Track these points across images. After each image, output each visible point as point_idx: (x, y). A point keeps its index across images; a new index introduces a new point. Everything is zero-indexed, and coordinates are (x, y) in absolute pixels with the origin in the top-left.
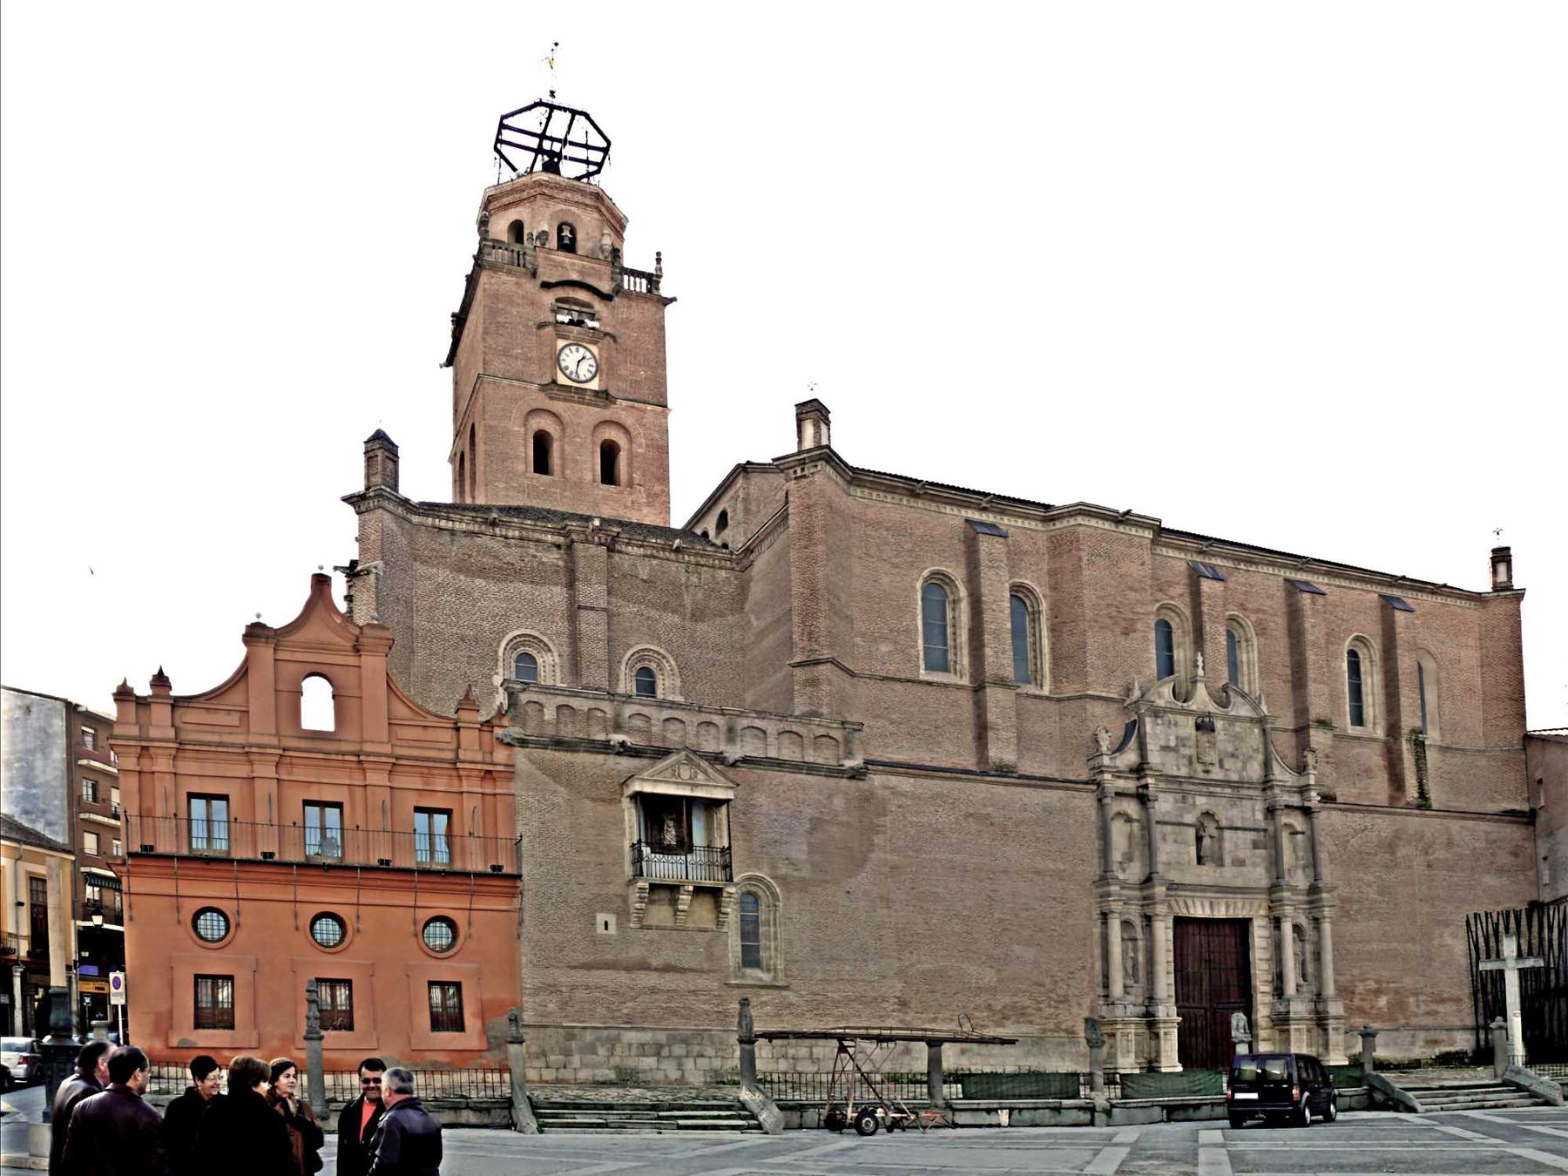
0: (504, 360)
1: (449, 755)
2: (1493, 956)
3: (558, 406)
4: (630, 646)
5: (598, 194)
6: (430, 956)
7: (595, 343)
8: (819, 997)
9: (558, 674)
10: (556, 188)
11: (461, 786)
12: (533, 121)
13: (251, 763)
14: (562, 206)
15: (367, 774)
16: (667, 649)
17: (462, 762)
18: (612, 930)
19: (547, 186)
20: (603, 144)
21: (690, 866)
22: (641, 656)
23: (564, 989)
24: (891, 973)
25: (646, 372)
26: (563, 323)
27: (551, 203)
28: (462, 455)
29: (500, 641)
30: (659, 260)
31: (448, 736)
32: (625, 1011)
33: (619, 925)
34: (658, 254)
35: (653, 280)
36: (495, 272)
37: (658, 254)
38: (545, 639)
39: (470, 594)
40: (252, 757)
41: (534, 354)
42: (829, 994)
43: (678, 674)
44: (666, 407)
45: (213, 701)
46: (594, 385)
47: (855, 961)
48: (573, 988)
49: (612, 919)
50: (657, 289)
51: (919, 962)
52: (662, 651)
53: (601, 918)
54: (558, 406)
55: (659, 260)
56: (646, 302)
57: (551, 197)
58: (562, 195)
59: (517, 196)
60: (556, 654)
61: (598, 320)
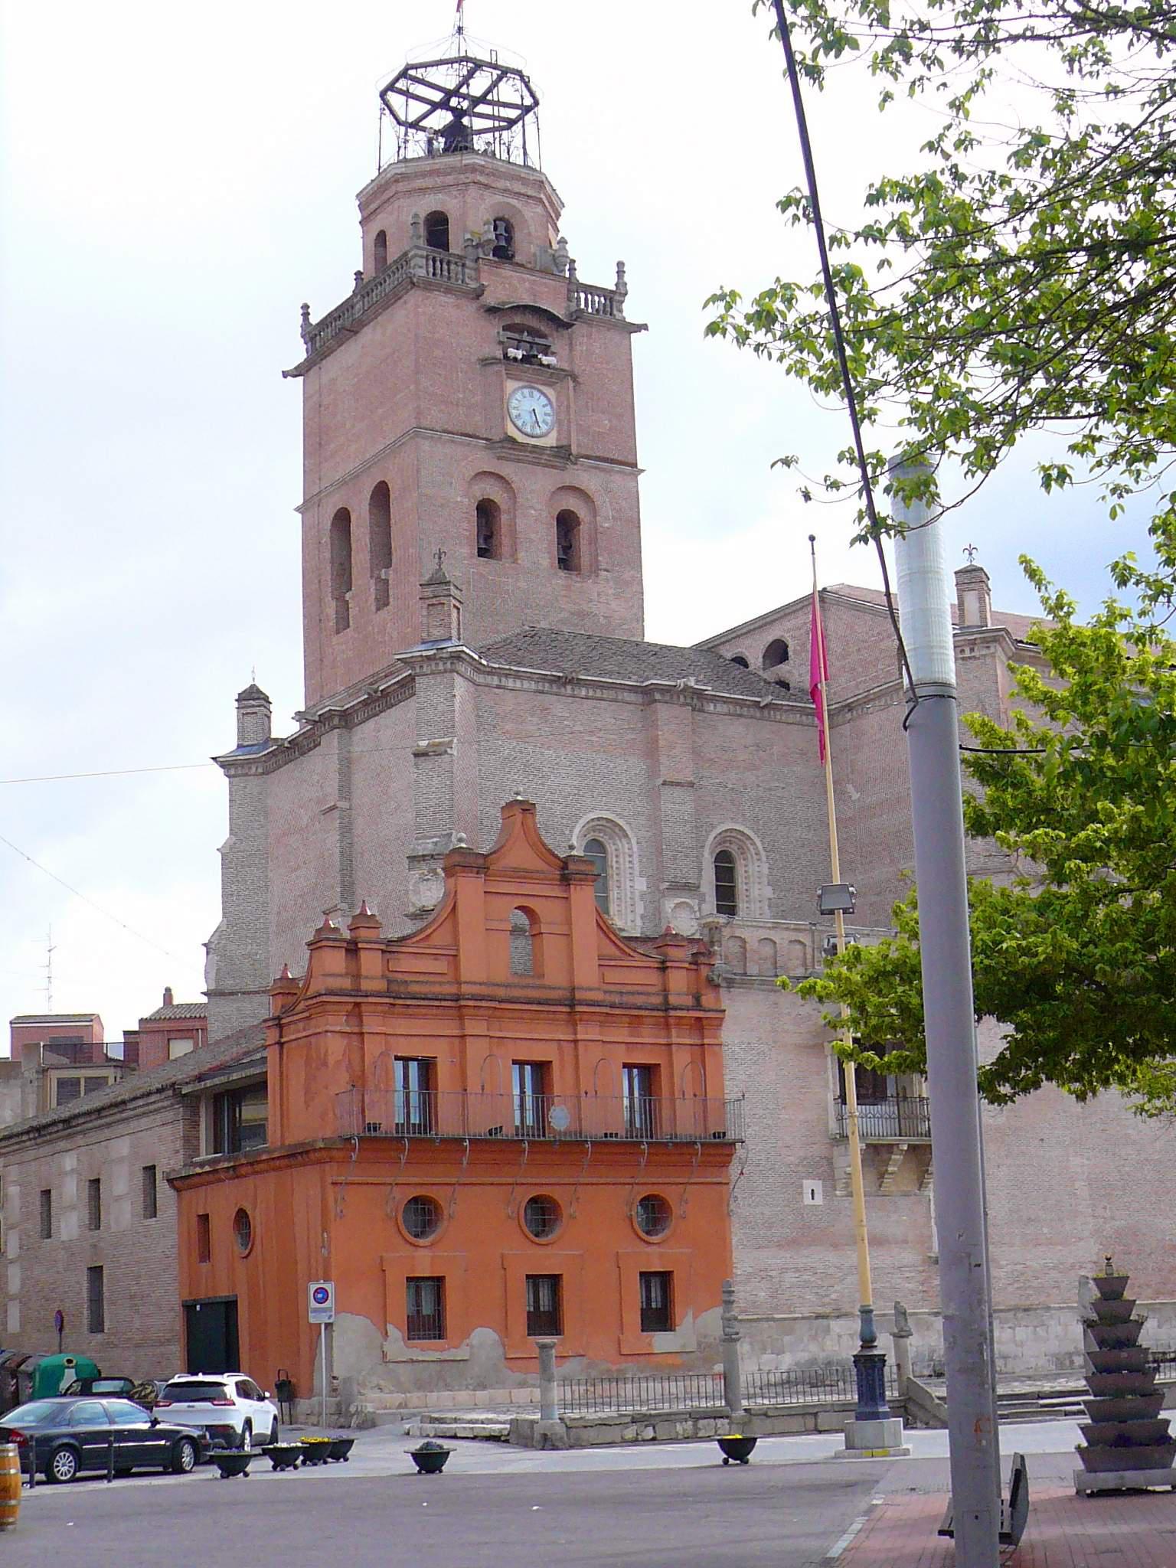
0: (443, 407)
1: (657, 1000)
2: (312, 947)
3: (507, 469)
4: (713, 827)
5: (542, 182)
6: (640, 1238)
7: (550, 385)
8: (1019, 1267)
9: (637, 866)
10: (494, 175)
11: (669, 1036)
12: (447, 78)
13: (461, 1018)
14: (499, 198)
15: (579, 1028)
16: (752, 829)
17: (675, 1009)
18: (819, 1200)
19: (482, 173)
20: (528, 101)
21: (902, 1121)
22: (726, 837)
23: (773, 1273)
24: (1086, 1233)
25: (610, 421)
26: (515, 359)
27: (487, 193)
28: (343, 518)
29: (574, 827)
30: (620, 273)
31: (653, 978)
32: (833, 1296)
33: (825, 1194)
34: (620, 265)
35: (614, 298)
36: (430, 291)
37: (620, 265)
38: (621, 822)
39: (539, 769)
40: (465, 1011)
41: (478, 398)
42: (1028, 1263)
43: (764, 859)
44: (635, 465)
45: (421, 945)
46: (551, 441)
47: (1051, 1220)
48: (784, 1270)
49: (817, 1185)
50: (621, 311)
51: (1113, 1218)
52: (746, 831)
53: (808, 1184)
54: (507, 469)
55: (620, 273)
56: (609, 330)
57: (487, 186)
58: (501, 184)
59: (439, 180)
60: (634, 841)
61: (553, 354)
